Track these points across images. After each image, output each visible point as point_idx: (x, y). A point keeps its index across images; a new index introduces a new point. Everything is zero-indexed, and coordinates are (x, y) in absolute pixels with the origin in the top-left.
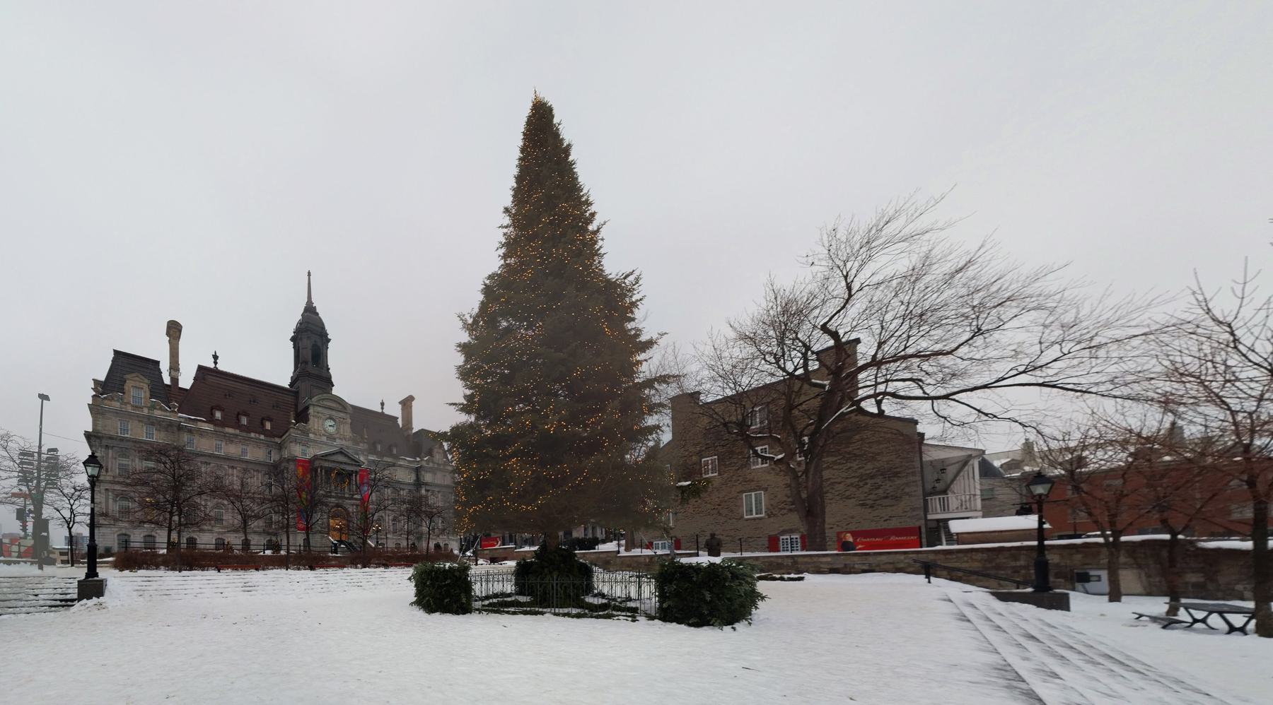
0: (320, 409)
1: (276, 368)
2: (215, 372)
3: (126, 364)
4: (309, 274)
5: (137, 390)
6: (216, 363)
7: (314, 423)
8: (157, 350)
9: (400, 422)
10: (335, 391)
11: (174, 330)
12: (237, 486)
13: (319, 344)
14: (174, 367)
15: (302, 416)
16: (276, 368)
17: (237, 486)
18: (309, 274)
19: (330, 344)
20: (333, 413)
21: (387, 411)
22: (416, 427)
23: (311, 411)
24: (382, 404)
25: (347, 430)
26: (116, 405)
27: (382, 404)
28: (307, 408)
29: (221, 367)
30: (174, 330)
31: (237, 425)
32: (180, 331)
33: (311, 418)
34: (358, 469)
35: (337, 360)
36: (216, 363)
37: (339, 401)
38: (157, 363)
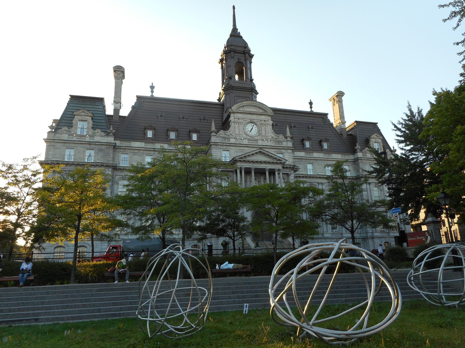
0: (240, 116)
1: (209, 89)
2: (152, 99)
3: (77, 102)
4: (234, 7)
5: (82, 126)
6: (311, 107)
7: (234, 128)
8: (103, 89)
9: (331, 118)
10: (260, 98)
11: (119, 72)
12: (393, 157)
13: (243, 60)
14: (117, 101)
15: (225, 125)
16: (209, 89)
17: (393, 157)
18: (234, 7)
19: (253, 60)
20: (254, 117)
21: (316, 109)
22: (349, 122)
23: (232, 118)
24: (311, 103)
25: (269, 131)
26: (65, 137)
27: (311, 103)
28: (229, 116)
29: (156, 95)
30: (119, 72)
31: (321, 149)
32: (123, 72)
33: (232, 124)
34: (280, 167)
35: (259, 72)
36: (311, 107)
37: (262, 106)
38: (102, 100)
